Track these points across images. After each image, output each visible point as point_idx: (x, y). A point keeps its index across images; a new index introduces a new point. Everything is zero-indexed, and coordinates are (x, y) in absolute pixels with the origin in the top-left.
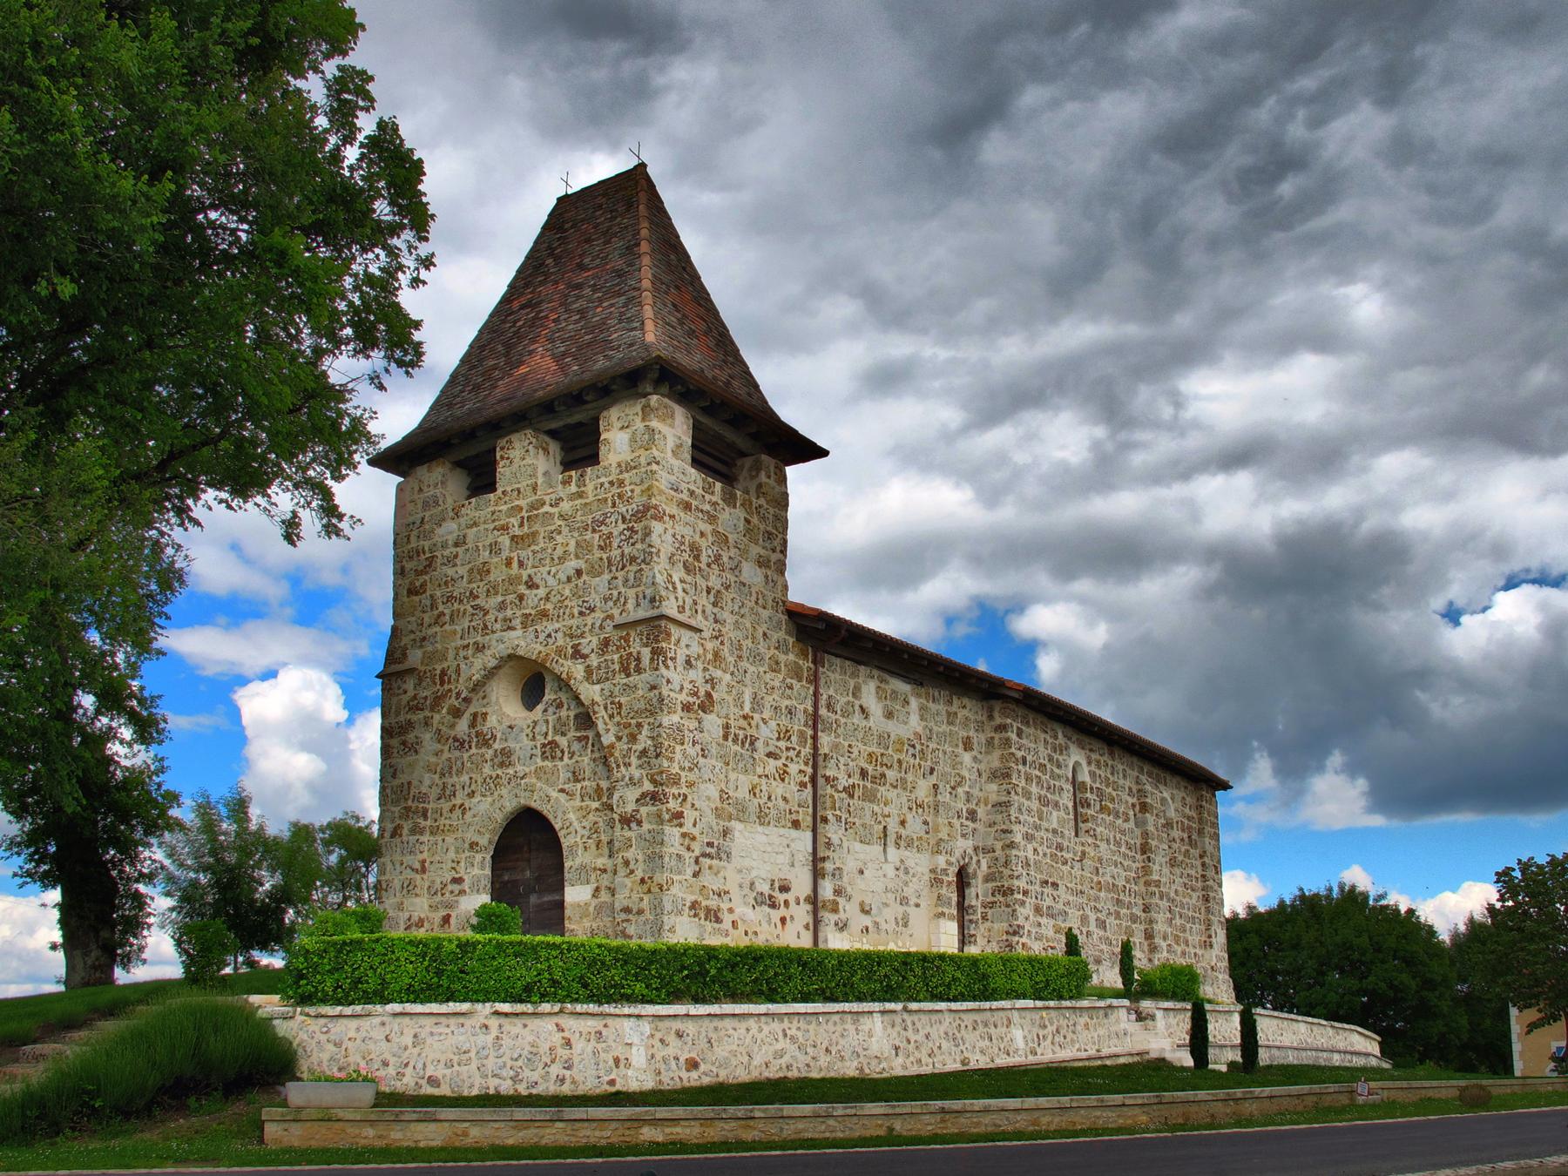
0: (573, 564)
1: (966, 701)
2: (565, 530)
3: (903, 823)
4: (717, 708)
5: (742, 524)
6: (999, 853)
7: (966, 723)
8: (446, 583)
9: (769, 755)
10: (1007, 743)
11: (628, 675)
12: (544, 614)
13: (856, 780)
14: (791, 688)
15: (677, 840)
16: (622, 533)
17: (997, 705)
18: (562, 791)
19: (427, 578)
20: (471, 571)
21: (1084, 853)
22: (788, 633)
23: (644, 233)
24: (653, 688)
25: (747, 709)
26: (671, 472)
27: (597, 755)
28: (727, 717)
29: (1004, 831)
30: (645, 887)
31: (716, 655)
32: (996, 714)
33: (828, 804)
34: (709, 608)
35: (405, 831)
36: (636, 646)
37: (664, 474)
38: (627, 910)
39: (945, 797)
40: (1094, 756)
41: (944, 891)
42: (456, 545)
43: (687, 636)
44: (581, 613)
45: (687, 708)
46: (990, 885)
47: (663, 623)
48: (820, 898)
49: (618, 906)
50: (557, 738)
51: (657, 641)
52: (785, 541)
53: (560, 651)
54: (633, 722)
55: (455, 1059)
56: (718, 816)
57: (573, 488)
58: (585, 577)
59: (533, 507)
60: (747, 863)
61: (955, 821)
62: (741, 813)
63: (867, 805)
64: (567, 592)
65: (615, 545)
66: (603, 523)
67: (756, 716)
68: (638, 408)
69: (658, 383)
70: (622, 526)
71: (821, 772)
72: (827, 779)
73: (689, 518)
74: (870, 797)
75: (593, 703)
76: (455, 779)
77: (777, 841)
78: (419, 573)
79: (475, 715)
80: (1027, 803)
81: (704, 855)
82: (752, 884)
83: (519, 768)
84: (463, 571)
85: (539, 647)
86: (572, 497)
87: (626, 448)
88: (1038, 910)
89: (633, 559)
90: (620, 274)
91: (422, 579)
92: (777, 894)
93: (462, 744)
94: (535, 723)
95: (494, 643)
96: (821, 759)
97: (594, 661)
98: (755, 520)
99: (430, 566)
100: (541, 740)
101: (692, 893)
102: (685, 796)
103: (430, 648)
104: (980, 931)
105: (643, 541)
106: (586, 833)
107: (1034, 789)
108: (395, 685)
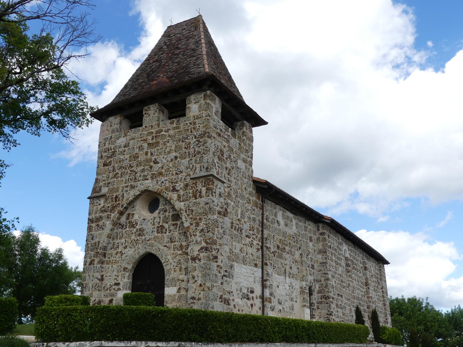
0: (174, 154)
1: (310, 222)
2: (171, 141)
3: (291, 268)
4: (229, 215)
5: (238, 145)
6: (323, 282)
7: (310, 231)
8: (120, 161)
9: (247, 236)
10: (325, 239)
11: (196, 199)
12: (161, 174)
13: (276, 249)
14: (254, 210)
15: (215, 268)
16: (194, 142)
17: (321, 225)
18: (165, 246)
19: (112, 159)
20: (130, 157)
21: (349, 284)
22: (253, 189)
23: (203, 36)
24: (207, 204)
26: (214, 121)
27: (181, 231)
29: (325, 274)
30: (202, 288)
31: (229, 194)
32: (320, 228)
33: (267, 258)
34: (227, 175)
35: (96, 262)
36: (200, 186)
37: (212, 121)
38: (193, 298)
39: (305, 259)
40: (350, 248)
41: (305, 296)
42: (125, 147)
43: (220, 184)
44: (176, 174)
45: (219, 213)
46: (320, 295)
47: (211, 178)
48: (265, 297)
49: (189, 296)
50: (164, 224)
51: (209, 185)
52: (252, 154)
53: (166, 189)
54: (198, 217)
56: (229, 260)
57: (175, 125)
58: (178, 159)
59: (157, 132)
60: (239, 280)
61: (308, 268)
62: (236, 259)
63: (279, 259)
64: (171, 165)
65: (192, 147)
66: (186, 138)
67: (242, 220)
68: (202, 95)
69: (210, 88)
70: (194, 140)
71: (265, 245)
72: (267, 248)
73: (219, 139)
74: (280, 257)
75: (181, 209)
76: (119, 241)
77: (249, 271)
78: (108, 157)
79: (129, 214)
80: (332, 263)
81: (225, 276)
82: (241, 289)
83: (147, 236)
84: (127, 157)
85: (158, 187)
86: (174, 128)
87: (197, 110)
88: (337, 305)
89: (199, 153)
90: (193, 50)
91: (110, 160)
92: (249, 294)
93: (123, 226)
94: (155, 218)
95: (139, 185)
96: (264, 240)
97: (181, 193)
98: (242, 144)
99: (113, 155)
100: (157, 225)
101: (220, 292)
102: (218, 249)
103: (112, 187)
104: (316, 313)
105: (203, 145)
106: (175, 264)
107: (334, 258)
108: (95, 202)
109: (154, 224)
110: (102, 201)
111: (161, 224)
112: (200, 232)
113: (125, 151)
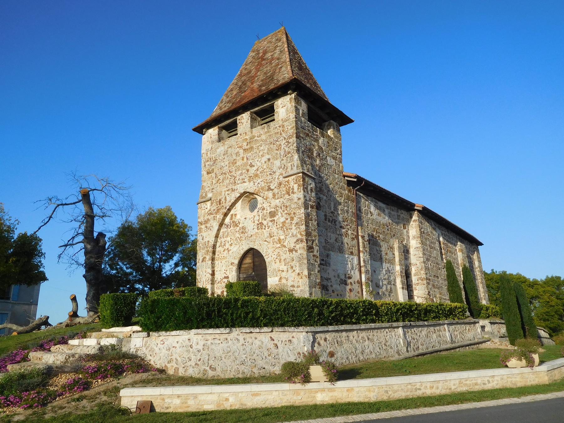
1: (403, 211)
2: (263, 145)
3: (386, 254)
12: (256, 175)
16: (284, 144)
18: (266, 241)
19: (214, 167)
20: (229, 163)
25: (332, 210)
27: (278, 226)
28: (326, 212)
40: (443, 232)
53: (262, 188)
54: (292, 213)
55: (223, 356)
56: (325, 249)
57: (266, 130)
58: (271, 161)
63: (374, 247)
64: (265, 167)
66: (277, 141)
70: (284, 141)
79: (232, 215)
84: (227, 163)
95: (238, 188)
97: (276, 191)
99: (215, 163)
100: (257, 222)
106: (275, 257)
108: (203, 206)
109: (254, 222)
110: (209, 203)
111: (260, 221)
112: (295, 226)
113: (224, 159)
